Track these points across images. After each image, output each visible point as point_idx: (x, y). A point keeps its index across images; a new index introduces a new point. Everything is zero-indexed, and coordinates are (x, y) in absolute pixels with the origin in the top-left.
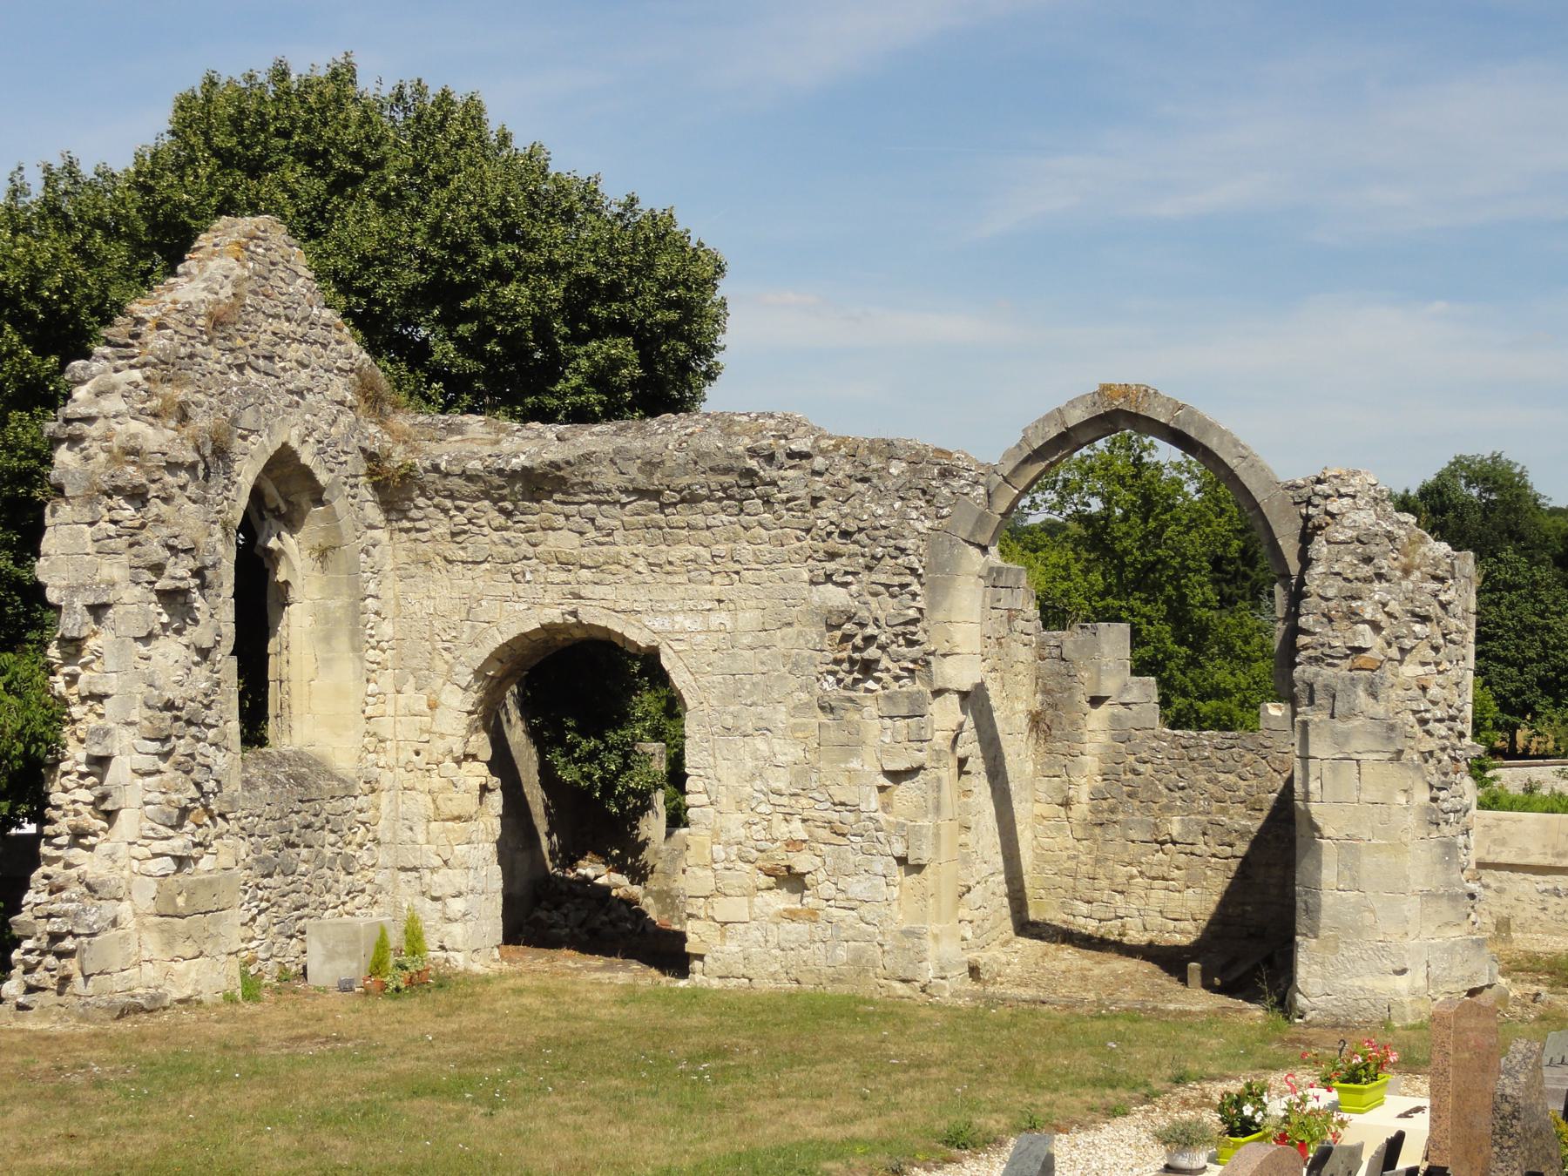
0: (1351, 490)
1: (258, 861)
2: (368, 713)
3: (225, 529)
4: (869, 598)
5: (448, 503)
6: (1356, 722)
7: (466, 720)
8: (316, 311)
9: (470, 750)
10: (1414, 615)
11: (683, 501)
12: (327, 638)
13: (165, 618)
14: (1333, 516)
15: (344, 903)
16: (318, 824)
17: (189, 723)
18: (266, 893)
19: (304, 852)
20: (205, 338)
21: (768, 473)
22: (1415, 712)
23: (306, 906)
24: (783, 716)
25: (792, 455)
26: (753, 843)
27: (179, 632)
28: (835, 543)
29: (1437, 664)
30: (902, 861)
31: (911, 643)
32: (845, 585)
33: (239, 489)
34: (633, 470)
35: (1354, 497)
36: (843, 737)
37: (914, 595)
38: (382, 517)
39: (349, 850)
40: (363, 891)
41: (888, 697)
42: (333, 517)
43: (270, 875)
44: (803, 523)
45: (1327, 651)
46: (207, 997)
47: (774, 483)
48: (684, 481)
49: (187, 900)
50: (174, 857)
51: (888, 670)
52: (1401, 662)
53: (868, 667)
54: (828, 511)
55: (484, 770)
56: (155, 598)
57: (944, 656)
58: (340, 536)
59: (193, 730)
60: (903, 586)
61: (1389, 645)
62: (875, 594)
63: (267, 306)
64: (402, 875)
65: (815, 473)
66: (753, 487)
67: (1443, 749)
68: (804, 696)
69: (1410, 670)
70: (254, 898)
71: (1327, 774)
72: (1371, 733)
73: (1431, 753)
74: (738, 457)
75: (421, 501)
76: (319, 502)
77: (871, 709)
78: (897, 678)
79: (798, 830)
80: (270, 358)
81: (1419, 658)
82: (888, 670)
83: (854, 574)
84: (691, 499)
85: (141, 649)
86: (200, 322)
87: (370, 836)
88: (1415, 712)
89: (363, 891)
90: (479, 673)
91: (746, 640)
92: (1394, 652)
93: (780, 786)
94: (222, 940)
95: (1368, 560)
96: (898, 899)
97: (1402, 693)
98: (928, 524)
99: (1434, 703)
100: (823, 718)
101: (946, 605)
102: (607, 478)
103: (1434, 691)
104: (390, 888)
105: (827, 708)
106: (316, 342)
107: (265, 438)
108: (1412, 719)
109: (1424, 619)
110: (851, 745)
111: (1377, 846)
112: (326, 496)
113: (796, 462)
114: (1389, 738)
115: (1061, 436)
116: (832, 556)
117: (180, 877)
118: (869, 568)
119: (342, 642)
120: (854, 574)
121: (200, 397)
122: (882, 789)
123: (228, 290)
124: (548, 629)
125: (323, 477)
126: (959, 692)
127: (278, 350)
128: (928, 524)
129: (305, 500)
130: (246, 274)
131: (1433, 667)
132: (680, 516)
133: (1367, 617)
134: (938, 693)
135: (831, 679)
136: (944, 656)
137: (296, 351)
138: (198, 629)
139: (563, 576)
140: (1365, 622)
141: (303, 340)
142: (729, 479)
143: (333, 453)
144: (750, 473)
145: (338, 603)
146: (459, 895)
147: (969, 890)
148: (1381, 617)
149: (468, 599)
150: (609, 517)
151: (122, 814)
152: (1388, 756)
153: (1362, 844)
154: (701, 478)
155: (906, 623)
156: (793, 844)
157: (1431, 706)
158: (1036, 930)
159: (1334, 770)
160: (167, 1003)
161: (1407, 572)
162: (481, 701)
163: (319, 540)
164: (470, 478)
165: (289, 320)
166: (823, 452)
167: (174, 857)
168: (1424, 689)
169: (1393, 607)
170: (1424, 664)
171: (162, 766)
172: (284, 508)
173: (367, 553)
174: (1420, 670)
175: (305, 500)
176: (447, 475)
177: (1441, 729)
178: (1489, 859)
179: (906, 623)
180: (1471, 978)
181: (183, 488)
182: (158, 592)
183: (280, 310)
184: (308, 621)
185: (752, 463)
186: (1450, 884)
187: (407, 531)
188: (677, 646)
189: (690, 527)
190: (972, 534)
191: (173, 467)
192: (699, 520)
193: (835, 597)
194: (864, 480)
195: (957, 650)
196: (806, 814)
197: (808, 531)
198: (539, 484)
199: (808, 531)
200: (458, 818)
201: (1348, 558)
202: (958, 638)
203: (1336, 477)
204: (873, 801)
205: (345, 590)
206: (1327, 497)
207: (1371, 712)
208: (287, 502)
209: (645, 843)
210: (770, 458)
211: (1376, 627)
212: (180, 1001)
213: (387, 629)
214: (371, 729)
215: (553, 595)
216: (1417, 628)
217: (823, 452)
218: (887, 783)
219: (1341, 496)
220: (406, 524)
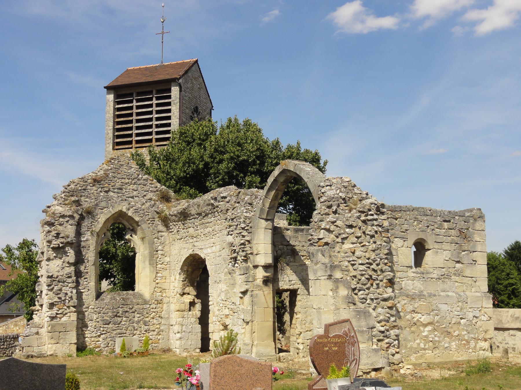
0: (329, 184)
1: (101, 320)
2: (157, 281)
3: (91, 233)
4: (236, 238)
5: (175, 223)
6: (318, 266)
7: (181, 283)
8: (140, 176)
9: (185, 292)
10: (347, 226)
11: (206, 215)
12: (144, 262)
13: (54, 255)
14: (323, 193)
15: (144, 334)
16: (131, 311)
17: (59, 282)
18: (105, 329)
19: (124, 319)
20: (91, 185)
21: (216, 204)
22: (349, 261)
23: (126, 333)
24: (223, 276)
25: (223, 198)
26: (219, 316)
27: (61, 258)
28: (230, 223)
29: (360, 243)
30: (243, 320)
31: (243, 251)
32: (231, 235)
33: (98, 222)
34: (196, 207)
35: (331, 186)
36: (232, 282)
37: (244, 236)
38: (165, 229)
39: (147, 319)
40: (154, 331)
41: (240, 268)
42: (142, 229)
43: (108, 324)
44: (224, 218)
45: (313, 241)
46: (60, 354)
47: (217, 207)
48: (204, 209)
49: (51, 328)
50: (50, 317)
51: (239, 260)
52: (343, 243)
53: (235, 259)
54: (229, 213)
55: (193, 297)
56: (51, 250)
57: (256, 255)
58: (145, 234)
59: (61, 283)
60: (240, 233)
61: (337, 237)
62: (237, 237)
63: (119, 176)
64: (171, 327)
65: (228, 202)
66: (214, 208)
67: (362, 275)
68: (226, 270)
69: (347, 246)
70: (99, 330)
71: (313, 286)
72: (322, 269)
73: (355, 277)
74: (209, 200)
75: (171, 224)
76: (139, 226)
77: (237, 273)
78: (241, 262)
79: (227, 312)
80: (121, 189)
81: (350, 241)
82: (239, 260)
83: (232, 231)
84: (207, 215)
85: (47, 263)
86: (89, 181)
87: (158, 316)
88: (349, 261)
89: (154, 331)
90: (181, 269)
91: (218, 254)
92: (339, 240)
93: (223, 298)
94: (67, 340)
95: (330, 207)
96: (244, 333)
97: (343, 254)
98: (252, 214)
99: (358, 258)
100: (230, 276)
101: (256, 239)
102: (193, 212)
103: (358, 253)
104: (167, 331)
105: (230, 273)
106: (140, 184)
107: (111, 209)
108: (347, 263)
109: (351, 227)
110: (234, 285)
111: (325, 311)
112: (139, 224)
113: (223, 199)
114: (326, 271)
115: (274, 180)
116: (230, 226)
117: (52, 322)
118: (236, 229)
119: (147, 263)
120: (232, 231)
121: (87, 200)
122: (241, 298)
123: (102, 172)
124: (191, 255)
125: (137, 219)
126: (262, 266)
127: (124, 187)
128: (252, 214)
129: (135, 225)
130: (110, 168)
131: (358, 244)
132: (207, 220)
133: (323, 227)
134: (256, 267)
135: (230, 264)
136: (256, 255)
137: (131, 187)
138: (69, 258)
139: (191, 241)
140: (322, 229)
141: (135, 184)
142: (210, 207)
143: (143, 212)
144: (212, 205)
145: (147, 252)
146: (178, 333)
147: (301, 333)
148: (332, 228)
149: (177, 250)
150: (197, 222)
151: (44, 306)
152: (327, 277)
153: (322, 310)
154: (206, 208)
155: (241, 245)
156: (227, 316)
157: (356, 259)
158: (80, 332)
159: (315, 284)
160: (46, 355)
161: (350, 211)
162: (186, 278)
163: (141, 236)
164: (175, 216)
165: (129, 179)
166: (231, 196)
167: (50, 317)
168: (353, 253)
169: (339, 223)
170: (353, 243)
171: (49, 293)
172: (131, 228)
173: (158, 239)
174: (352, 246)
175: (135, 225)
176: (172, 216)
177: (362, 268)
178: (499, 326)
179: (241, 245)
180: (372, 364)
181: (67, 222)
182: (52, 248)
183: (125, 176)
184: (140, 257)
185: (212, 201)
186: (360, 327)
187: (171, 232)
188: (208, 258)
189: (208, 223)
190: (260, 215)
191: (63, 216)
192: (209, 220)
193: (230, 239)
194: (239, 203)
195: (260, 253)
196: (229, 306)
197: (226, 219)
198: (184, 216)
199: (226, 219)
200: (178, 311)
201: (323, 207)
202: (260, 249)
203: (327, 180)
204: (238, 301)
205: (148, 249)
206: (323, 187)
207: (323, 261)
208: (132, 226)
209: (285, 322)
210: (215, 199)
211: (329, 231)
212: (50, 355)
213: (167, 259)
214: (159, 285)
215: (191, 246)
216: (348, 230)
217: (231, 196)
218: (242, 296)
219: (327, 186)
220: (170, 230)
